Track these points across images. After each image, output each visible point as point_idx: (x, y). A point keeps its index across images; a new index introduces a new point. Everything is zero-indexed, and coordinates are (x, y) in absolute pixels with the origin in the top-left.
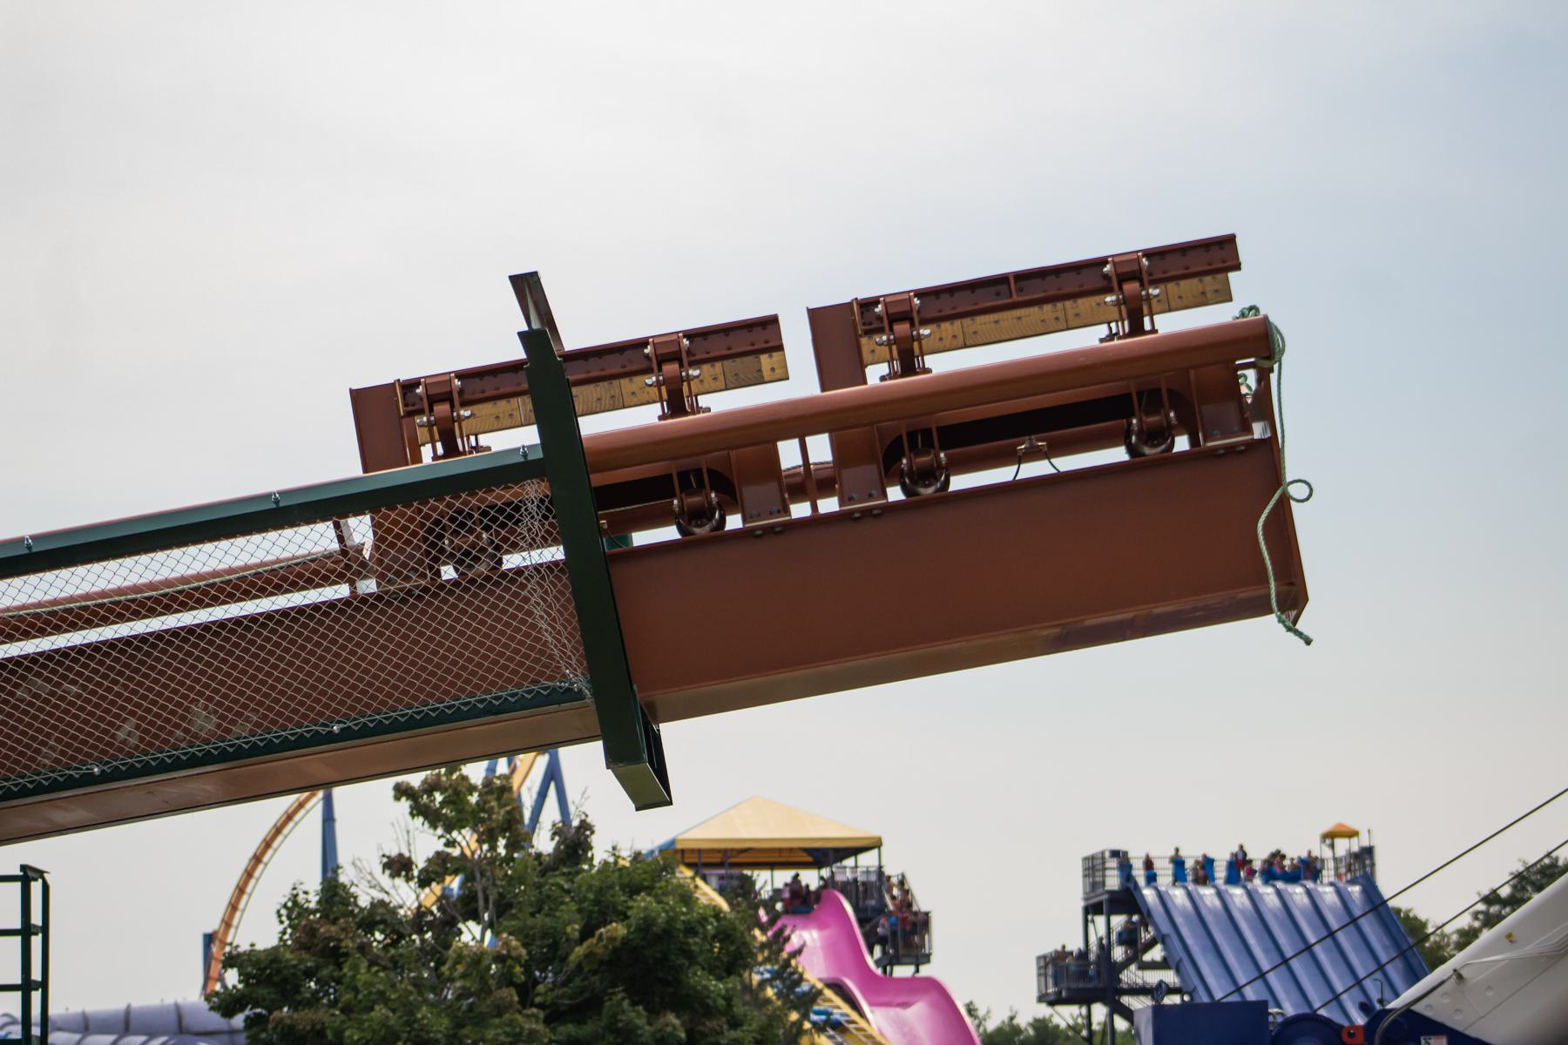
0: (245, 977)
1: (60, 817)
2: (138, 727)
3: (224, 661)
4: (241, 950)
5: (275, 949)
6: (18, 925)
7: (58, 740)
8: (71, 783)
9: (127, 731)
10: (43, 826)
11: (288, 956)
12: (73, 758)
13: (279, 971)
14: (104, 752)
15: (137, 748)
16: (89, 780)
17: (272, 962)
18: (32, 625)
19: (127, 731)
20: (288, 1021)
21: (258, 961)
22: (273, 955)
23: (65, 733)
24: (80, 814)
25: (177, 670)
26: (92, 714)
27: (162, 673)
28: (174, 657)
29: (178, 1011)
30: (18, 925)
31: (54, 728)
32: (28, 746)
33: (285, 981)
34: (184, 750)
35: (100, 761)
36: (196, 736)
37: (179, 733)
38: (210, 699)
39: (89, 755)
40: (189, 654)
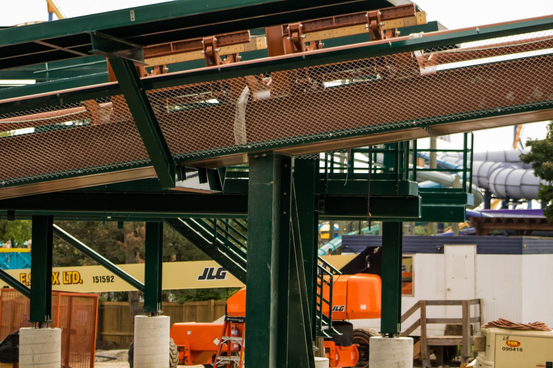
0: (533, 150)
1: (484, 124)
2: (514, 95)
3: (546, 74)
4: (532, 140)
5: (545, 140)
6: (462, 148)
7: (486, 100)
8: (490, 115)
9: (510, 96)
10: (478, 127)
11: (549, 143)
12: (491, 106)
13: (545, 148)
14: (502, 104)
15: (513, 103)
16: (496, 113)
17: (543, 145)
18: (477, 54)
19: (510, 96)
20: (548, 167)
21: (539, 145)
22: (544, 142)
23: (488, 97)
24: (492, 124)
25: (530, 76)
26: (498, 91)
27: (524, 77)
28: (528, 72)
29: (505, 155)
30: (462, 148)
31: (485, 95)
32: (474, 97)
33: (548, 152)
34: (531, 104)
35: (500, 107)
36: (535, 99)
37: (529, 98)
38: (541, 87)
39: (497, 105)
40: (534, 71)
